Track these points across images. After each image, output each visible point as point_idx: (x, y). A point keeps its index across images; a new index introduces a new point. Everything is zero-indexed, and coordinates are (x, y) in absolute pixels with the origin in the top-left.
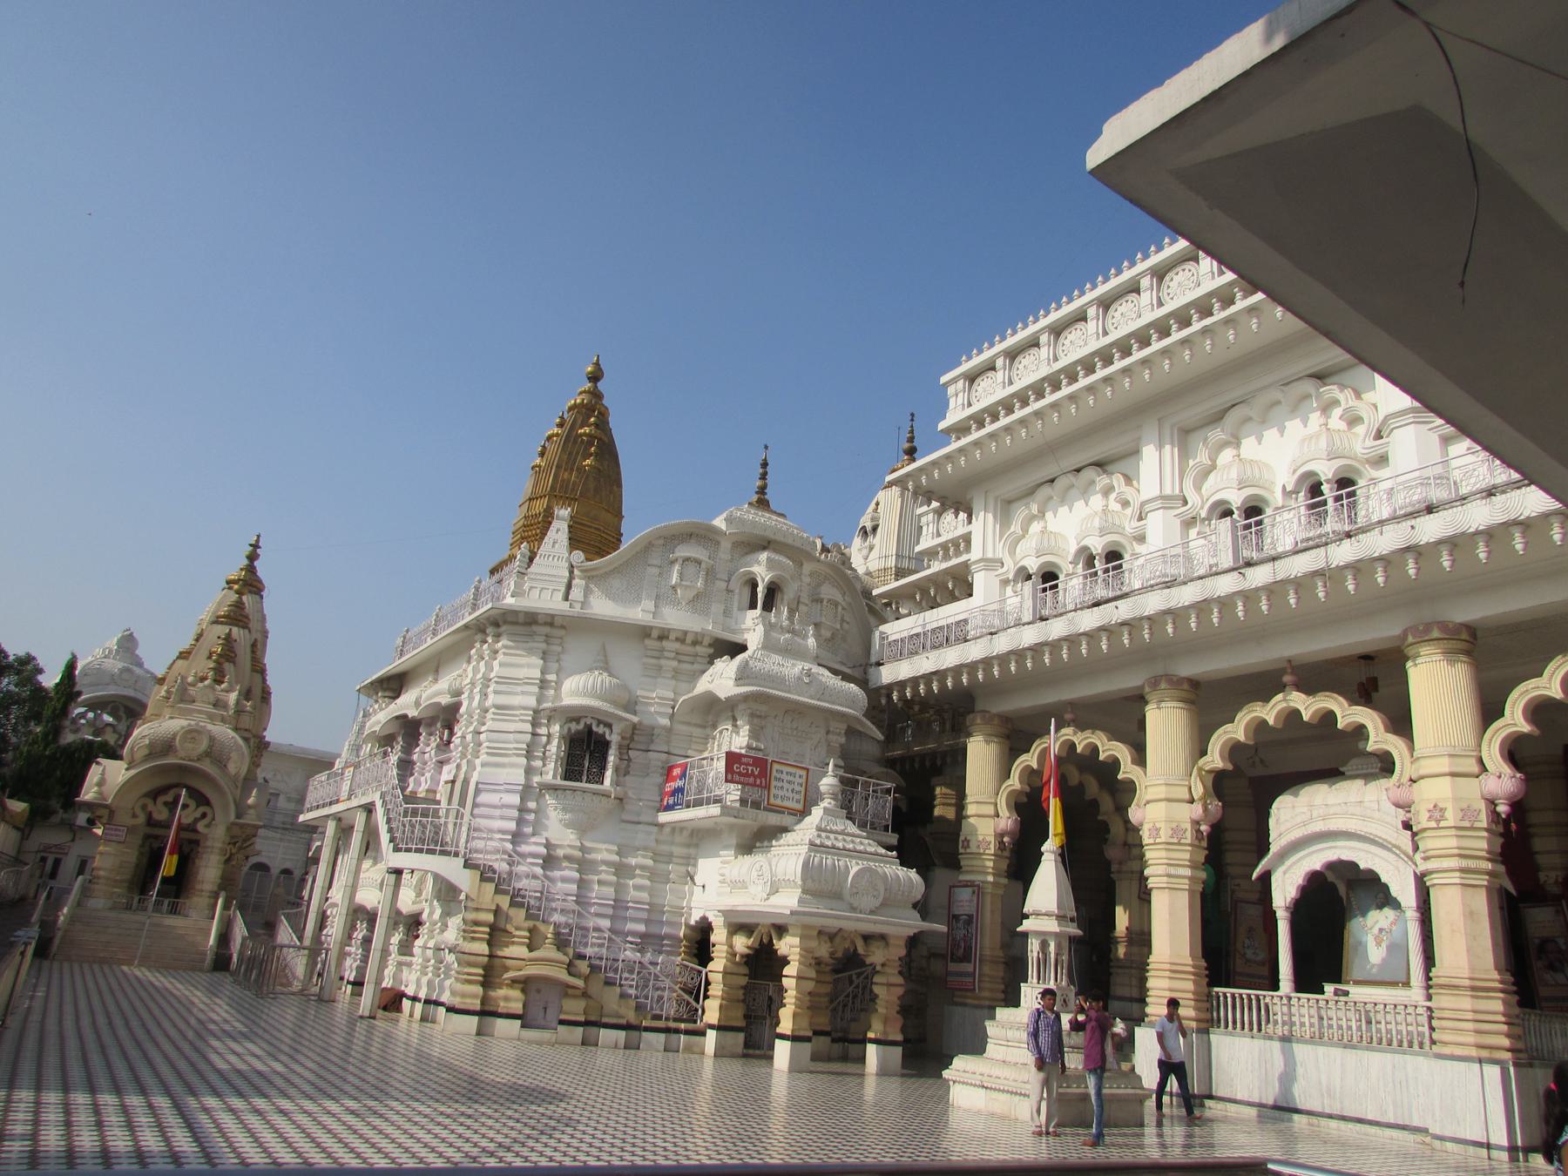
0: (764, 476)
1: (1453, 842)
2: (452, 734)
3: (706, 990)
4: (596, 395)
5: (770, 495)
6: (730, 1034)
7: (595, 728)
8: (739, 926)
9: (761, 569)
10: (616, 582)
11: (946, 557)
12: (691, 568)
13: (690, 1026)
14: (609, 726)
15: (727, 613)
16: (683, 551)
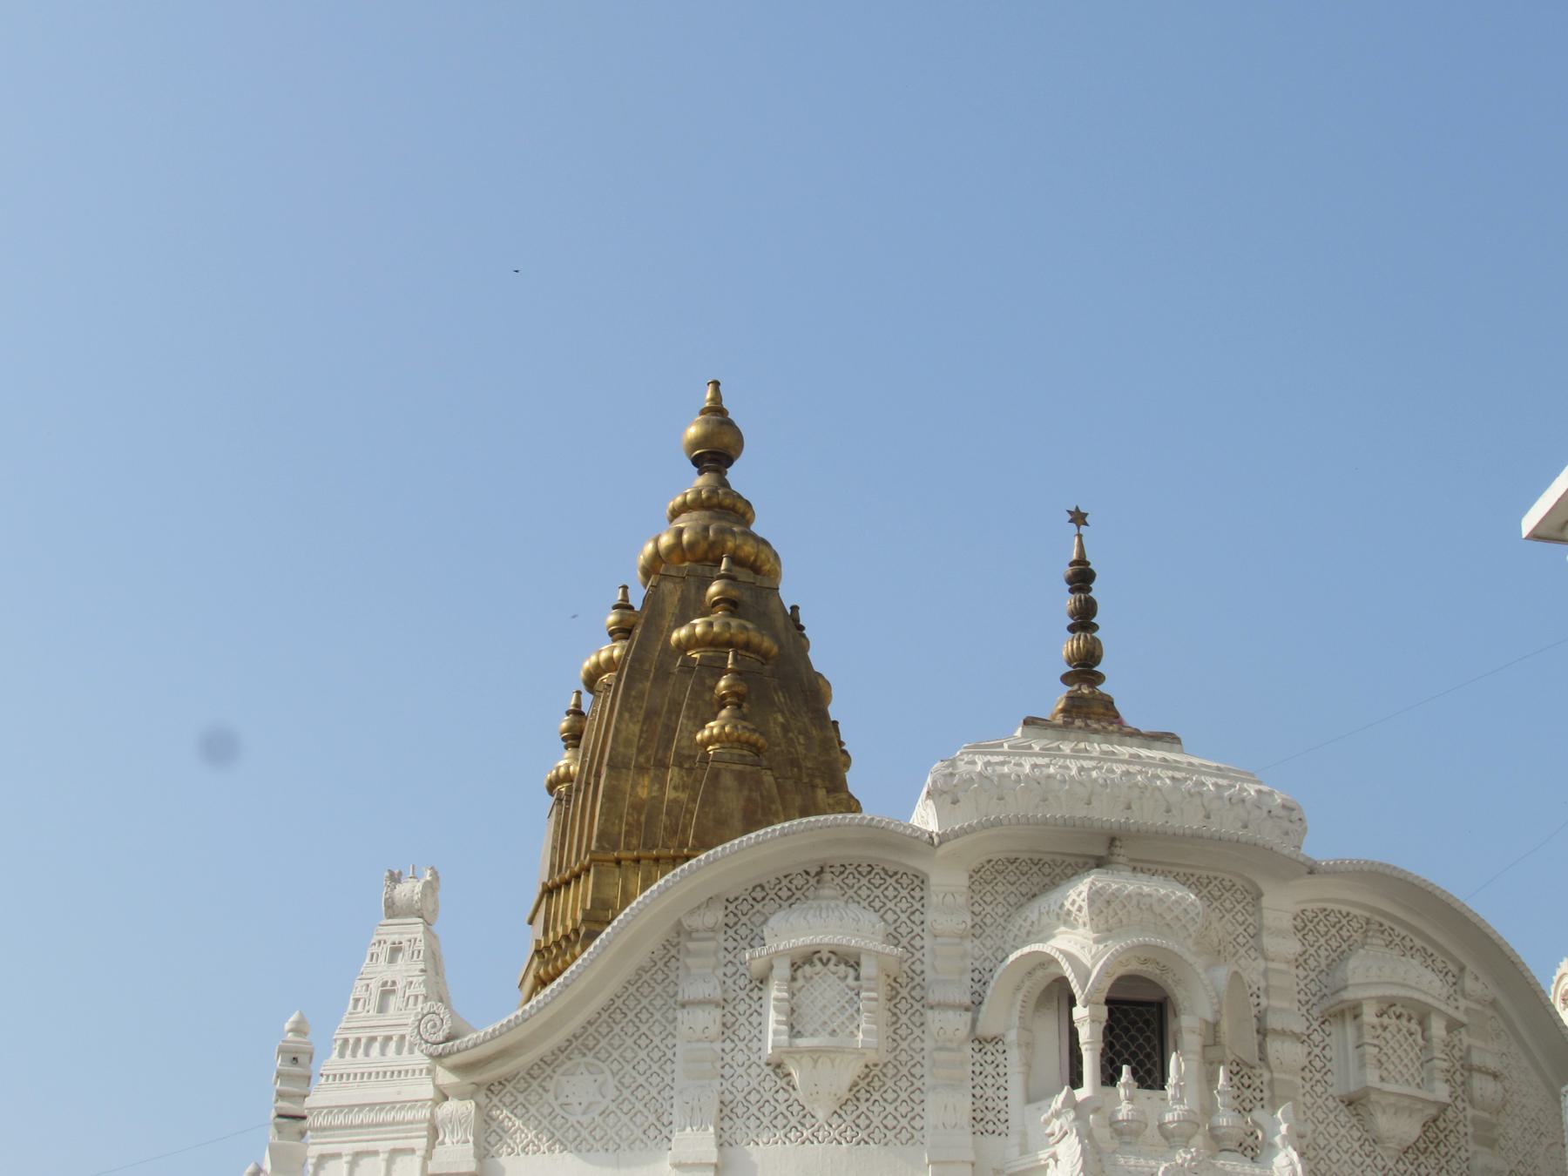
0: (1084, 619)
4: (726, 509)
5: (1116, 681)
9: (1077, 939)
10: (579, 1088)
12: (826, 987)
15: (986, 1119)
16: (790, 932)
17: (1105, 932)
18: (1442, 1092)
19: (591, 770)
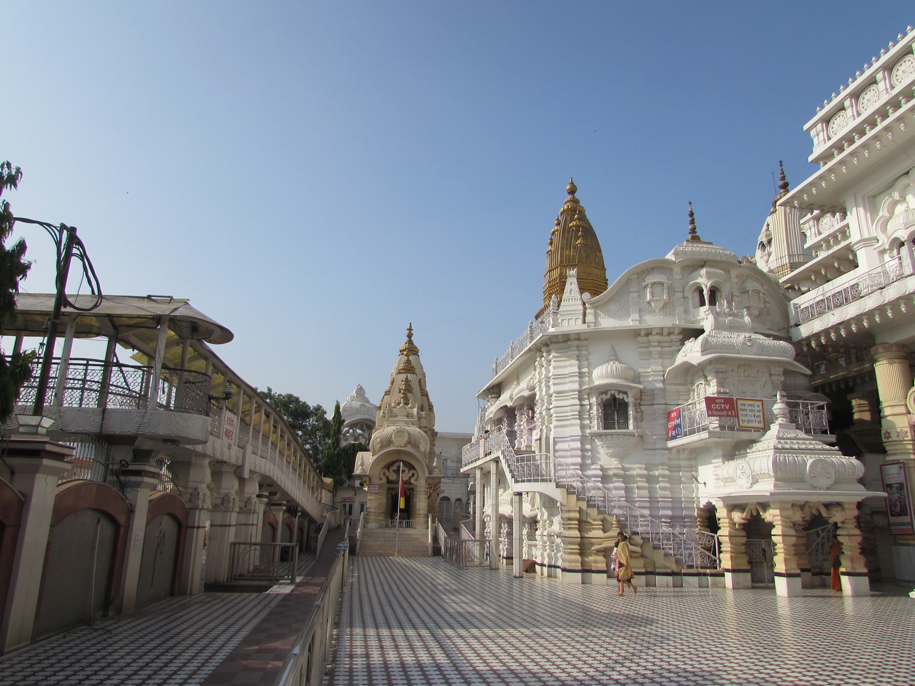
0: (692, 222)
2: (534, 412)
3: (719, 548)
4: (575, 201)
5: (699, 233)
6: (741, 575)
7: (617, 396)
8: (734, 505)
9: (703, 280)
10: (612, 307)
11: (829, 247)
12: (658, 289)
14: (626, 393)
15: (686, 312)
16: (650, 279)
17: (709, 278)
18: (762, 306)
19: (557, 250)
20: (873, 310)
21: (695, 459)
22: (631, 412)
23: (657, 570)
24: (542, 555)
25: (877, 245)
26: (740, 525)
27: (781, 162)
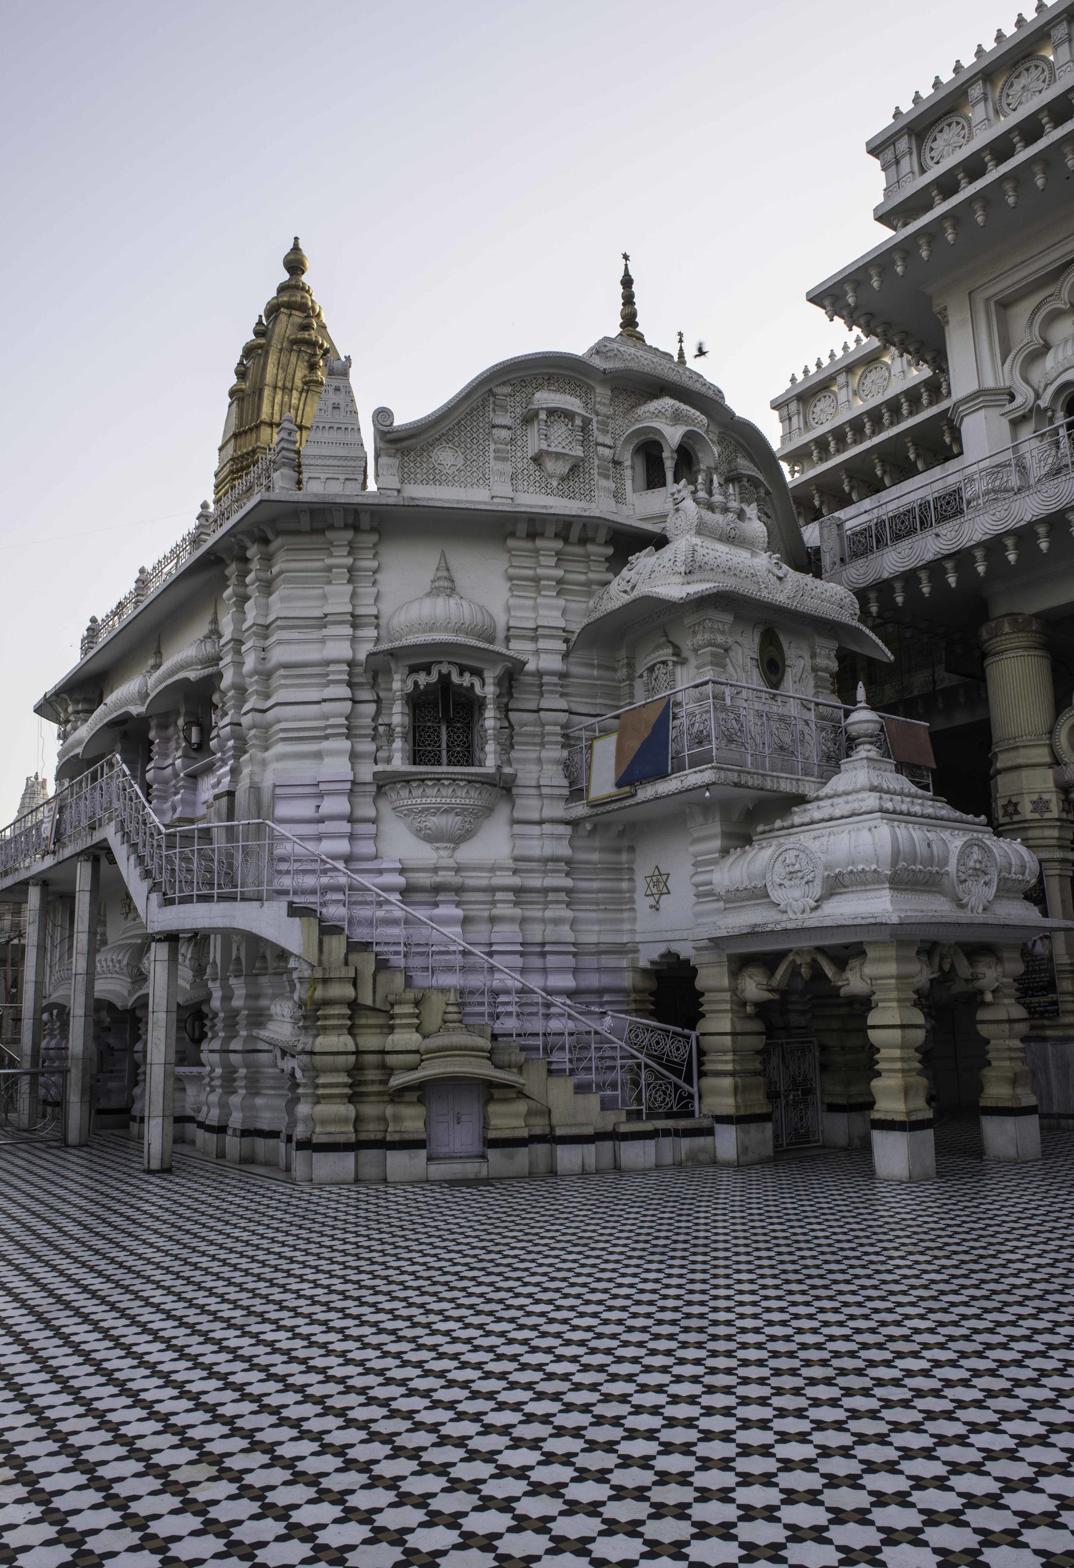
1: (1055, 833)
2: (206, 730)
3: (701, 1064)
6: (753, 1127)
7: (455, 679)
8: (749, 956)
11: (825, 455)
13: (683, 1124)
14: (478, 673)
20: (1031, 525)
21: (631, 849)
22: (489, 723)
23: (559, 1132)
24: (223, 1106)
25: (1009, 407)
26: (756, 1004)
27: (680, 334)
